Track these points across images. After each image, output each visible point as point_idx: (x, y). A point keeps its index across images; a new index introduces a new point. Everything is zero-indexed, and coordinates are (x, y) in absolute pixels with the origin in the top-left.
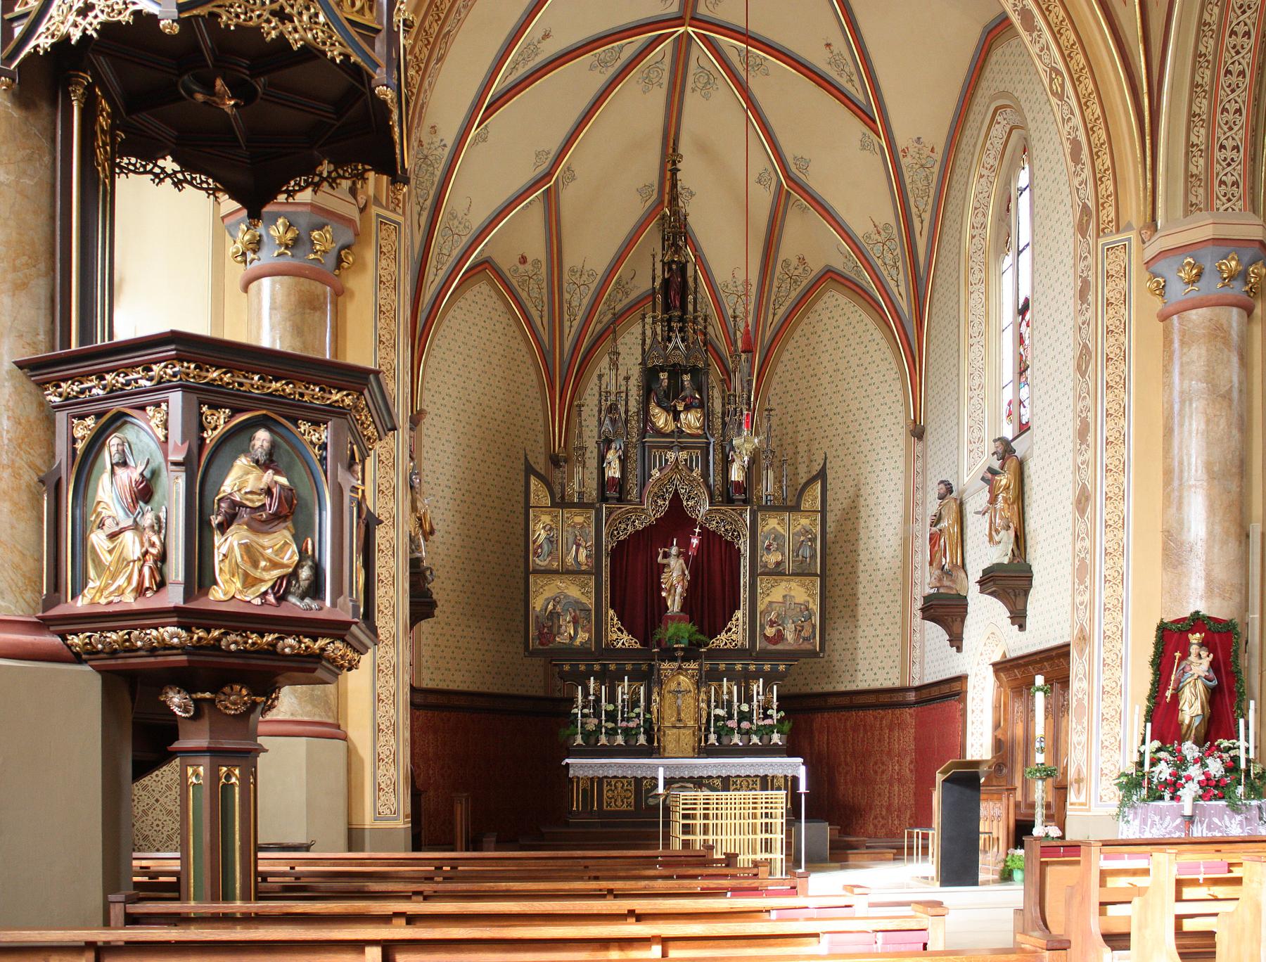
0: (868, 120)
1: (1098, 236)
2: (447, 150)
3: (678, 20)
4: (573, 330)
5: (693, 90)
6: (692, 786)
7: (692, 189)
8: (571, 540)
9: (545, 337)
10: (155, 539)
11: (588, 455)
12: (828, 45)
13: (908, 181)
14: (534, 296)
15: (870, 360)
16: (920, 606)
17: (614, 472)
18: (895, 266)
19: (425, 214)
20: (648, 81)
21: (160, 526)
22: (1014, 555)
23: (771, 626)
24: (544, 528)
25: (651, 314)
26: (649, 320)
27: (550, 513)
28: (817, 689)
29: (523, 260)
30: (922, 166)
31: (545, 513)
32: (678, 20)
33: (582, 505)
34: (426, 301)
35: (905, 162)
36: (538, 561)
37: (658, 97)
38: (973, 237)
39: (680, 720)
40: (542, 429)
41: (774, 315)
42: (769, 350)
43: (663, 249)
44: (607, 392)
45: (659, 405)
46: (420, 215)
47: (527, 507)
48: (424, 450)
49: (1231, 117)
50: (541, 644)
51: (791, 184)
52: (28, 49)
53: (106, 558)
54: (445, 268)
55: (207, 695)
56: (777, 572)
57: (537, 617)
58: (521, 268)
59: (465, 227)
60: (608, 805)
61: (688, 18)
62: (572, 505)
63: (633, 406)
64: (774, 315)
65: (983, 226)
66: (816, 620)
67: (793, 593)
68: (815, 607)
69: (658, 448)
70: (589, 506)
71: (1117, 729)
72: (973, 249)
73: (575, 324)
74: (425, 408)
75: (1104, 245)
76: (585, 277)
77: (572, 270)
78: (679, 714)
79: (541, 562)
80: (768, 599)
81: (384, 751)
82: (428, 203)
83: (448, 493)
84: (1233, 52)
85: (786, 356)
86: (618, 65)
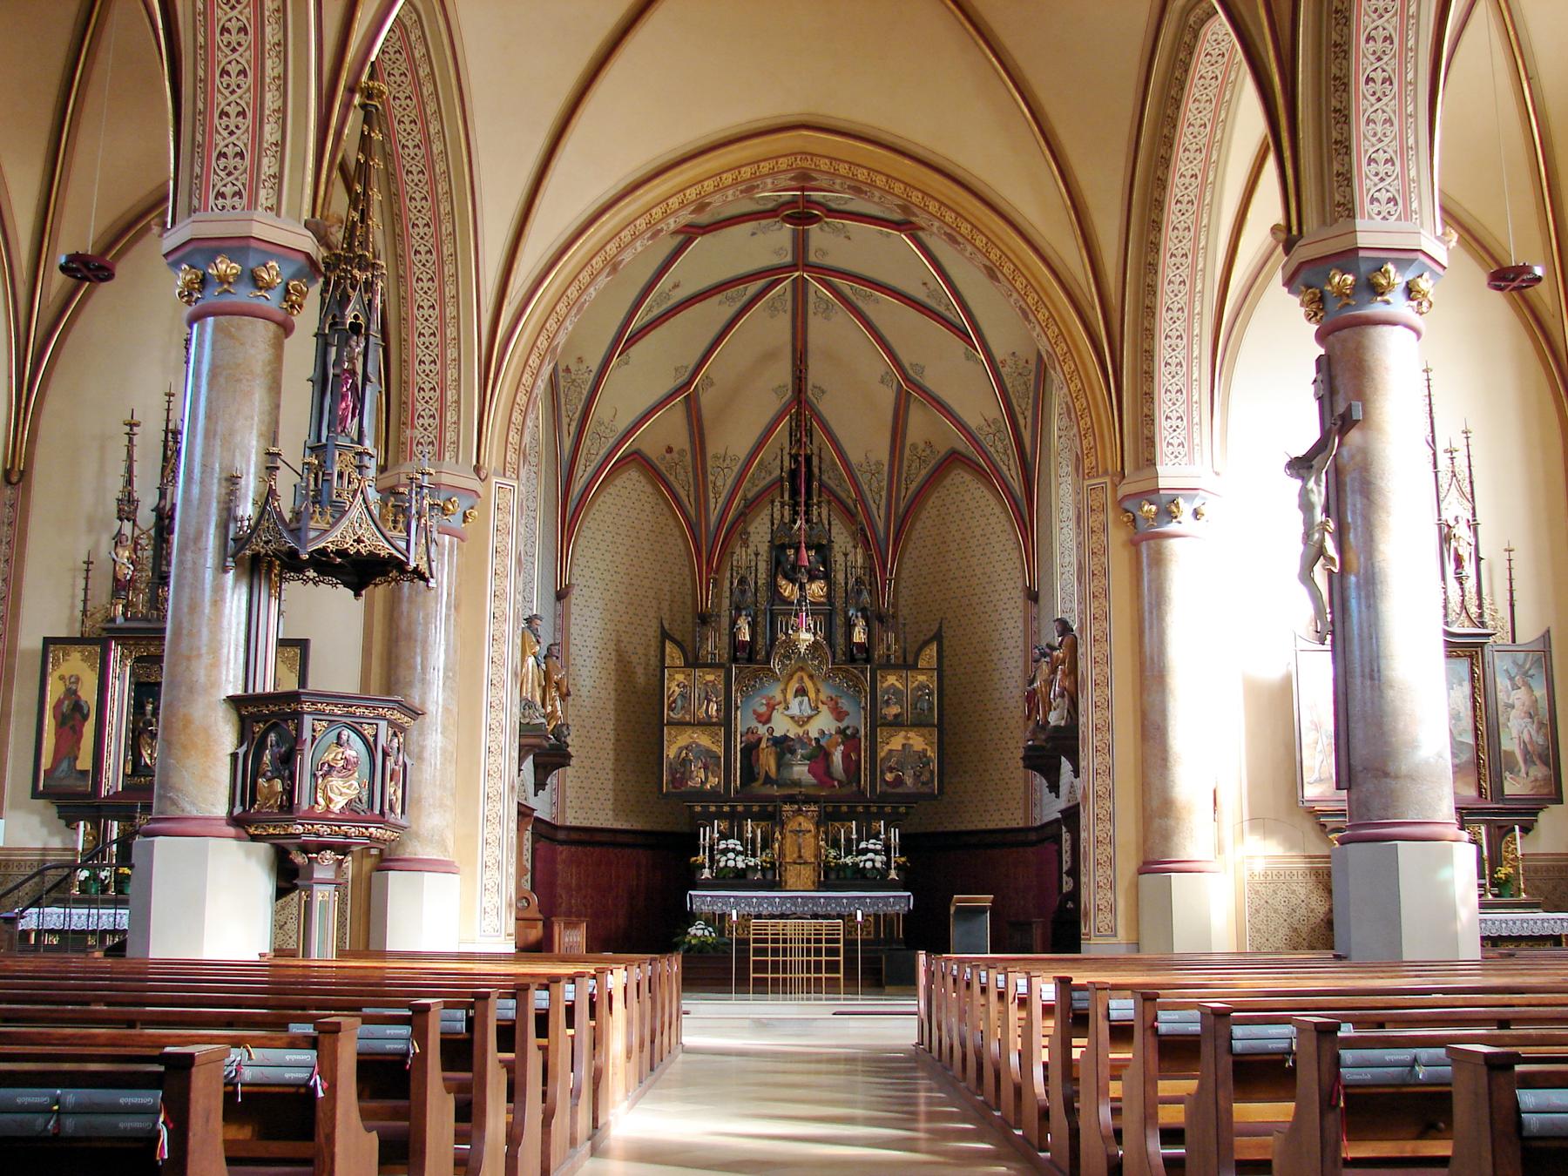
0: (965, 336)
1: (1084, 479)
2: (592, 375)
3: (793, 267)
5: (815, 314)
7: (823, 387)
8: (703, 695)
9: (692, 512)
11: (723, 619)
12: (925, 284)
13: (1009, 386)
14: (681, 482)
15: (991, 531)
16: (1021, 755)
17: (746, 636)
19: (574, 424)
20: (772, 307)
23: (891, 772)
24: (678, 685)
25: (779, 499)
26: (777, 503)
27: (683, 673)
28: (951, 828)
29: (670, 450)
30: (1020, 374)
32: (793, 267)
34: (575, 493)
35: (1004, 371)
36: (671, 714)
37: (784, 322)
38: (1060, 437)
39: (800, 857)
40: (690, 592)
41: (907, 489)
42: (903, 521)
44: (737, 567)
45: (786, 577)
48: (573, 617)
49: (1173, 396)
50: (675, 787)
54: (593, 465)
56: (897, 723)
57: (671, 764)
58: (668, 456)
61: (801, 266)
62: (706, 665)
64: (907, 489)
66: (934, 766)
67: (911, 742)
70: (720, 666)
71: (1109, 872)
72: (1061, 447)
73: (721, 501)
75: (1088, 486)
76: (728, 461)
77: (716, 457)
78: (800, 851)
79: (676, 716)
80: (889, 747)
81: (489, 907)
82: (577, 415)
83: (595, 653)
84: (1170, 350)
86: (745, 299)
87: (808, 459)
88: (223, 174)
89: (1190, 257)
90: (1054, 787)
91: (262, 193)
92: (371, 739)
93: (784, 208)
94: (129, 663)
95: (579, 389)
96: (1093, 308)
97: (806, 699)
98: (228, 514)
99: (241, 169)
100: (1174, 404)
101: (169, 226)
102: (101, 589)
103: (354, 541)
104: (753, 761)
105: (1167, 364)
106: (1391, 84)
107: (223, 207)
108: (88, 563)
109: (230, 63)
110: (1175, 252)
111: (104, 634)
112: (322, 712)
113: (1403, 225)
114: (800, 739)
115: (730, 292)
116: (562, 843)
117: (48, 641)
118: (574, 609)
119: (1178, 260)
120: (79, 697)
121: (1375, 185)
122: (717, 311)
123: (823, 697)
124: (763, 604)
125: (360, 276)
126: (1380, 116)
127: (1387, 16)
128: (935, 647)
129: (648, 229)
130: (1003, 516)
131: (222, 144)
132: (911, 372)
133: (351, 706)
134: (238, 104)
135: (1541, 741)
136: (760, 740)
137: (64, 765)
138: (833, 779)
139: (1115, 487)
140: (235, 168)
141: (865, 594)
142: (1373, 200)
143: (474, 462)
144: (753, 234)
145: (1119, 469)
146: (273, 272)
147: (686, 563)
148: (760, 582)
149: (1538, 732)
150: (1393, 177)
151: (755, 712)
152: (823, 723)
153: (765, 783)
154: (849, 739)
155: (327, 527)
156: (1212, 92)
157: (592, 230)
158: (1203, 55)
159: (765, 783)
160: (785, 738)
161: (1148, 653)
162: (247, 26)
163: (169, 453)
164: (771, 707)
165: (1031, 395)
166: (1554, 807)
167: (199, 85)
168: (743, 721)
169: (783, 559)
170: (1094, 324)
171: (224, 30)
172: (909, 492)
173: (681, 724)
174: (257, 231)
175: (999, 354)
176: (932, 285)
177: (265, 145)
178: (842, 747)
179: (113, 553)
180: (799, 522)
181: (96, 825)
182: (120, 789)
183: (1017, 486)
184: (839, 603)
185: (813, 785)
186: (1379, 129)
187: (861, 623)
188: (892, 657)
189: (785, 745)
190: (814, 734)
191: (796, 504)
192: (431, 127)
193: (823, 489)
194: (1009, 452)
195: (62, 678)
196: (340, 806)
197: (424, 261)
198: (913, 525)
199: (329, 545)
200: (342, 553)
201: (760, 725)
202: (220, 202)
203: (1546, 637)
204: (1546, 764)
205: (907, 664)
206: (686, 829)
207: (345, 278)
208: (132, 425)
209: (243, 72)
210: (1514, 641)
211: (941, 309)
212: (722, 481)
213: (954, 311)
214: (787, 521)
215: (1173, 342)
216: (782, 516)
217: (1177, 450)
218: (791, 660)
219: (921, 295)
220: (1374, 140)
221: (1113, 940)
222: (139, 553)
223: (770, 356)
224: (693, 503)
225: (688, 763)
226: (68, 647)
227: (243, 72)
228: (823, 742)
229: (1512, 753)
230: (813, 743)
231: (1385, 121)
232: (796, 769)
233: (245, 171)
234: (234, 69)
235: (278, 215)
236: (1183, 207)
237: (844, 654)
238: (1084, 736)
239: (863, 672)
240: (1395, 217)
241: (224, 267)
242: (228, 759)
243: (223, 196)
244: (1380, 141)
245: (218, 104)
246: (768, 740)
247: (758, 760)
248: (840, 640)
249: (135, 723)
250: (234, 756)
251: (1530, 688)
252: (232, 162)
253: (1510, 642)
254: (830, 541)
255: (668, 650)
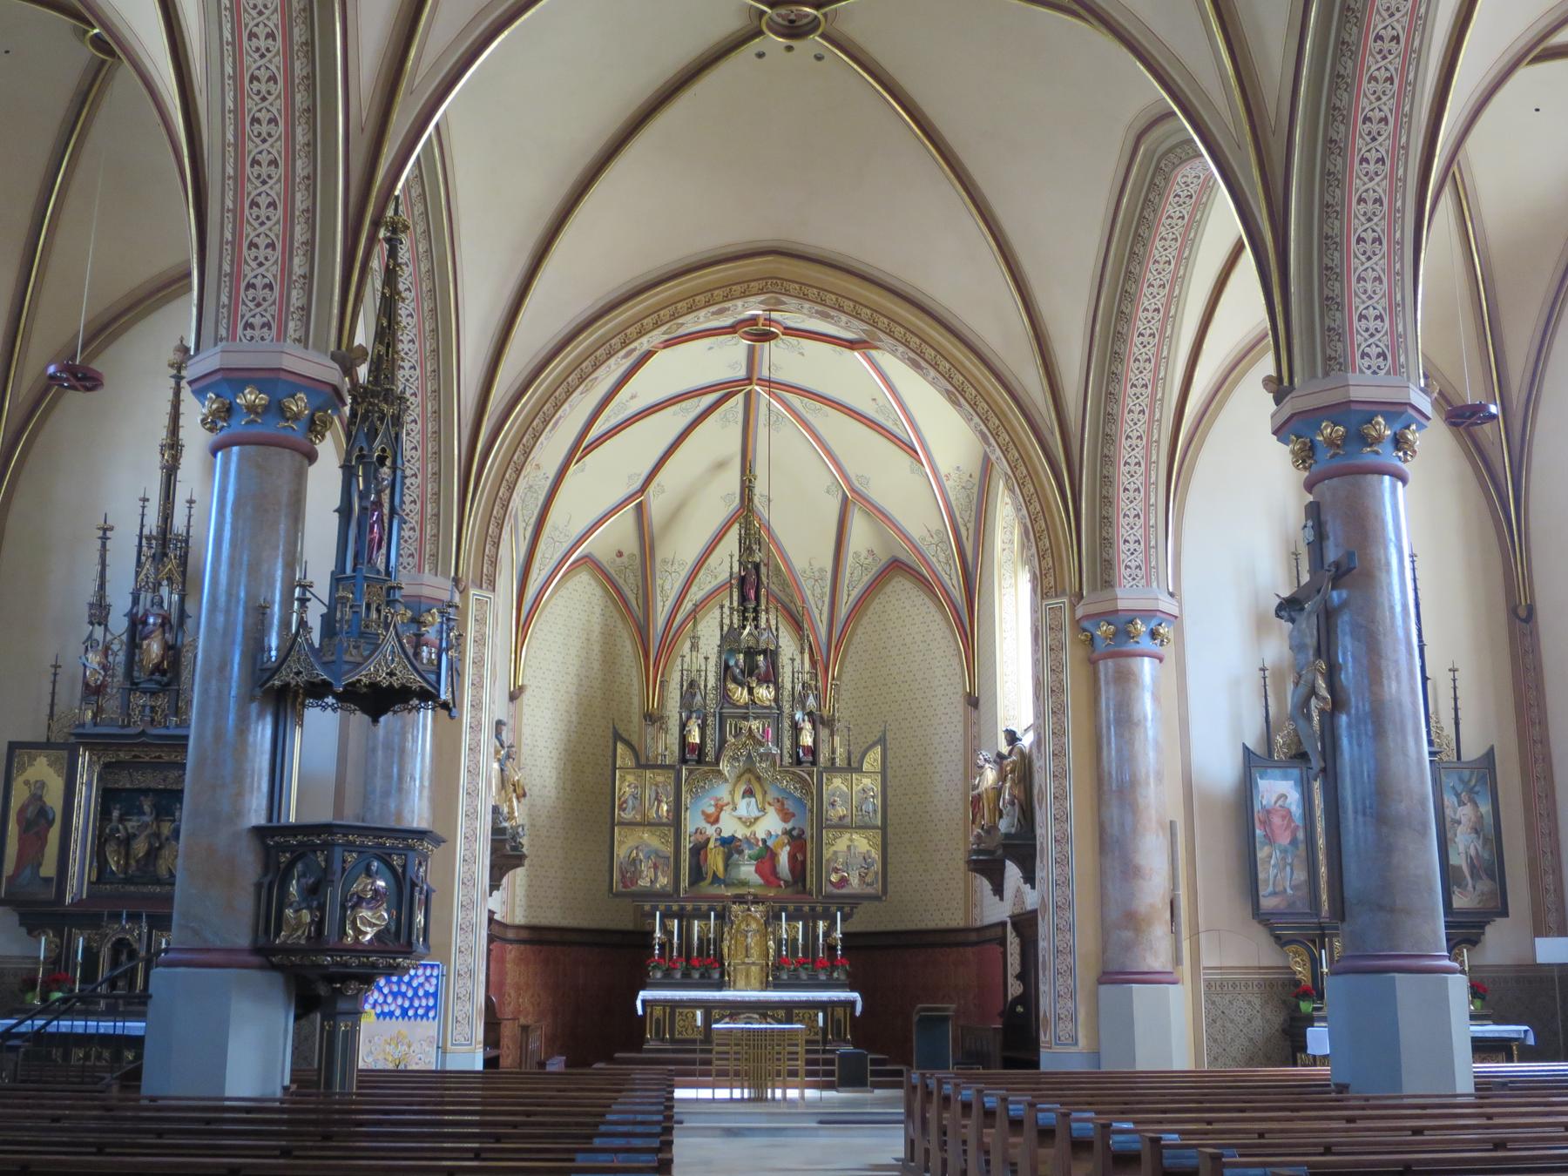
1: (1042, 598)
4: (666, 609)
6: (756, 1016)
8: (653, 796)
10: (318, 914)
12: (874, 400)
17: (695, 738)
18: (947, 563)
21: (321, 907)
22: (1021, 825)
24: (629, 786)
29: (620, 554)
31: (628, 773)
33: (663, 767)
35: (948, 484)
38: (1004, 550)
43: (740, 551)
44: (687, 670)
46: (525, 529)
47: (614, 768)
49: (1131, 520)
51: (855, 495)
52: (268, 685)
53: (293, 922)
55: (338, 985)
56: (842, 826)
58: (618, 560)
59: (565, 535)
60: (680, 1033)
61: (755, 381)
63: (712, 682)
64: (849, 595)
65: (1011, 542)
67: (856, 843)
68: (875, 854)
69: (733, 717)
74: (526, 682)
75: (1046, 605)
76: (676, 566)
77: (664, 561)
79: (628, 816)
85: (860, 631)
87: (757, 567)
88: (251, 305)
89: (1150, 387)
90: (998, 890)
91: (291, 325)
92: (400, 870)
93: (743, 324)
94: (97, 769)
95: (535, 495)
96: (1053, 433)
97: (753, 800)
98: (256, 644)
99: (270, 300)
100: (1132, 528)
101: (192, 353)
102: (70, 696)
103: (387, 674)
104: (702, 863)
105: (1126, 490)
106: (1381, 244)
107: (252, 338)
108: (56, 667)
109: (259, 194)
110: (1136, 382)
111: (72, 740)
112: (352, 843)
113: (1393, 380)
114: (747, 839)
115: (683, 404)
116: (511, 942)
117: (13, 747)
118: (526, 710)
119: (1138, 390)
120: (44, 803)
121: (1366, 340)
122: (672, 421)
123: (769, 798)
124: (712, 706)
125: (389, 410)
126: (1371, 275)
127: (1377, 179)
128: (879, 749)
129: (623, 348)
130: (943, 624)
131: (251, 275)
132: (856, 483)
133: (381, 837)
134: (267, 236)
135: (1486, 856)
136: (708, 840)
137: (27, 872)
138: (779, 879)
139: (1073, 607)
140: (264, 299)
141: (811, 697)
142: (1364, 355)
143: (453, 574)
144: (711, 348)
145: (1077, 590)
146: (299, 404)
147: (633, 664)
148: (709, 687)
149: (1483, 847)
150: (1382, 333)
151: (703, 813)
152: (771, 825)
153: (712, 883)
154: (796, 840)
155: (359, 659)
156: (1178, 231)
157: (569, 348)
158: (1172, 196)
159: (712, 883)
160: (733, 838)
161: (1106, 769)
162: (278, 159)
163: (143, 558)
164: (719, 808)
165: (974, 508)
166: (1500, 921)
167: (226, 214)
168: (693, 822)
169: (732, 663)
170: (1054, 450)
171: (255, 162)
172: (851, 598)
173: (631, 824)
174: (288, 363)
175: (943, 469)
176: (880, 401)
177: (294, 278)
178: (788, 848)
179: (84, 658)
180: (748, 628)
181: (59, 934)
182: (84, 896)
183: (958, 595)
184: (786, 707)
185: (761, 885)
186: (1369, 286)
187: (808, 726)
188: (837, 760)
189: (732, 845)
190: (761, 835)
191: (745, 610)
192: (420, 246)
193: (770, 598)
194: (951, 562)
195: (27, 783)
196: (368, 937)
197: (407, 376)
198: (854, 629)
199: (363, 678)
200: (374, 686)
201: (708, 826)
202: (249, 332)
203: (1490, 754)
204: (1492, 878)
205: (853, 767)
206: (627, 923)
207: (373, 412)
208: (105, 530)
209: (272, 204)
210: (1459, 757)
211: (889, 425)
212: (667, 587)
213: (900, 426)
214: (736, 626)
215: (1132, 468)
216: (732, 622)
217: (1134, 572)
218: (739, 761)
219: (869, 410)
220: (1364, 297)
221: (1073, 1049)
222: (111, 658)
223: (721, 465)
224: (641, 606)
225: (638, 862)
226: (33, 751)
227: (272, 204)
228: (769, 843)
229: (1459, 868)
230: (760, 844)
231: (1375, 279)
232: (744, 869)
233: (274, 303)
234: (264, 201)
235: (306, 347)
236: (1145, 339)
237: (791, 756)
238: (1042, 843)
239: (810, 774)
240: (1384, 371)
241: (253, 397)
242: (251, 889)
243: (252, 326)
244: (1370, 298)
245: (248, 236)
246: (716, 840)
247: (706, 860)
248: (787, 743)
249: (102, 829)
250: (259, 886)
251: (1476, 805)
252: (261, 293)
253: (1455, 759)
254: (778, 647)
255: (619, 751)
